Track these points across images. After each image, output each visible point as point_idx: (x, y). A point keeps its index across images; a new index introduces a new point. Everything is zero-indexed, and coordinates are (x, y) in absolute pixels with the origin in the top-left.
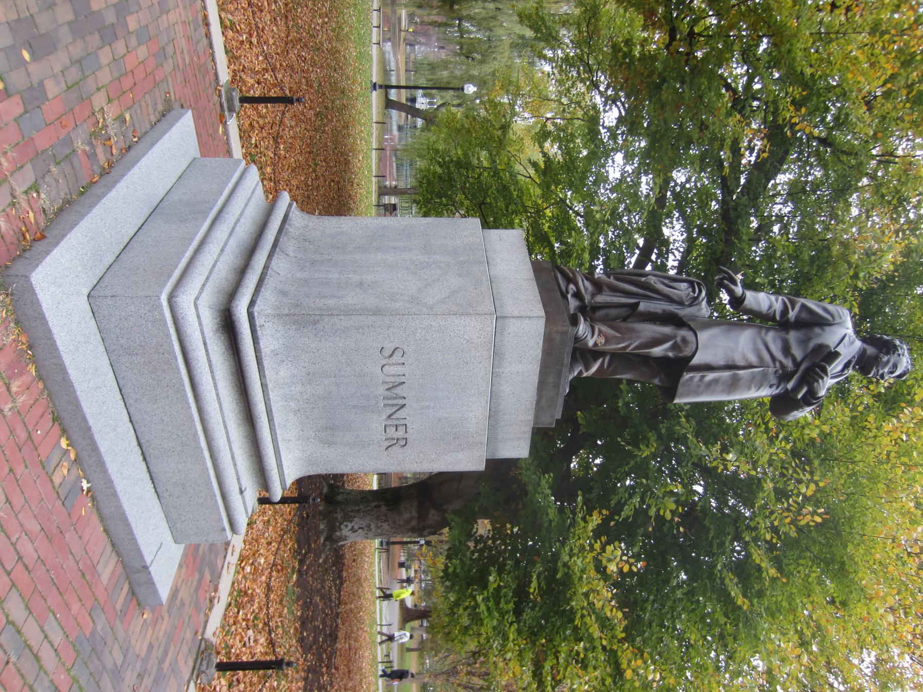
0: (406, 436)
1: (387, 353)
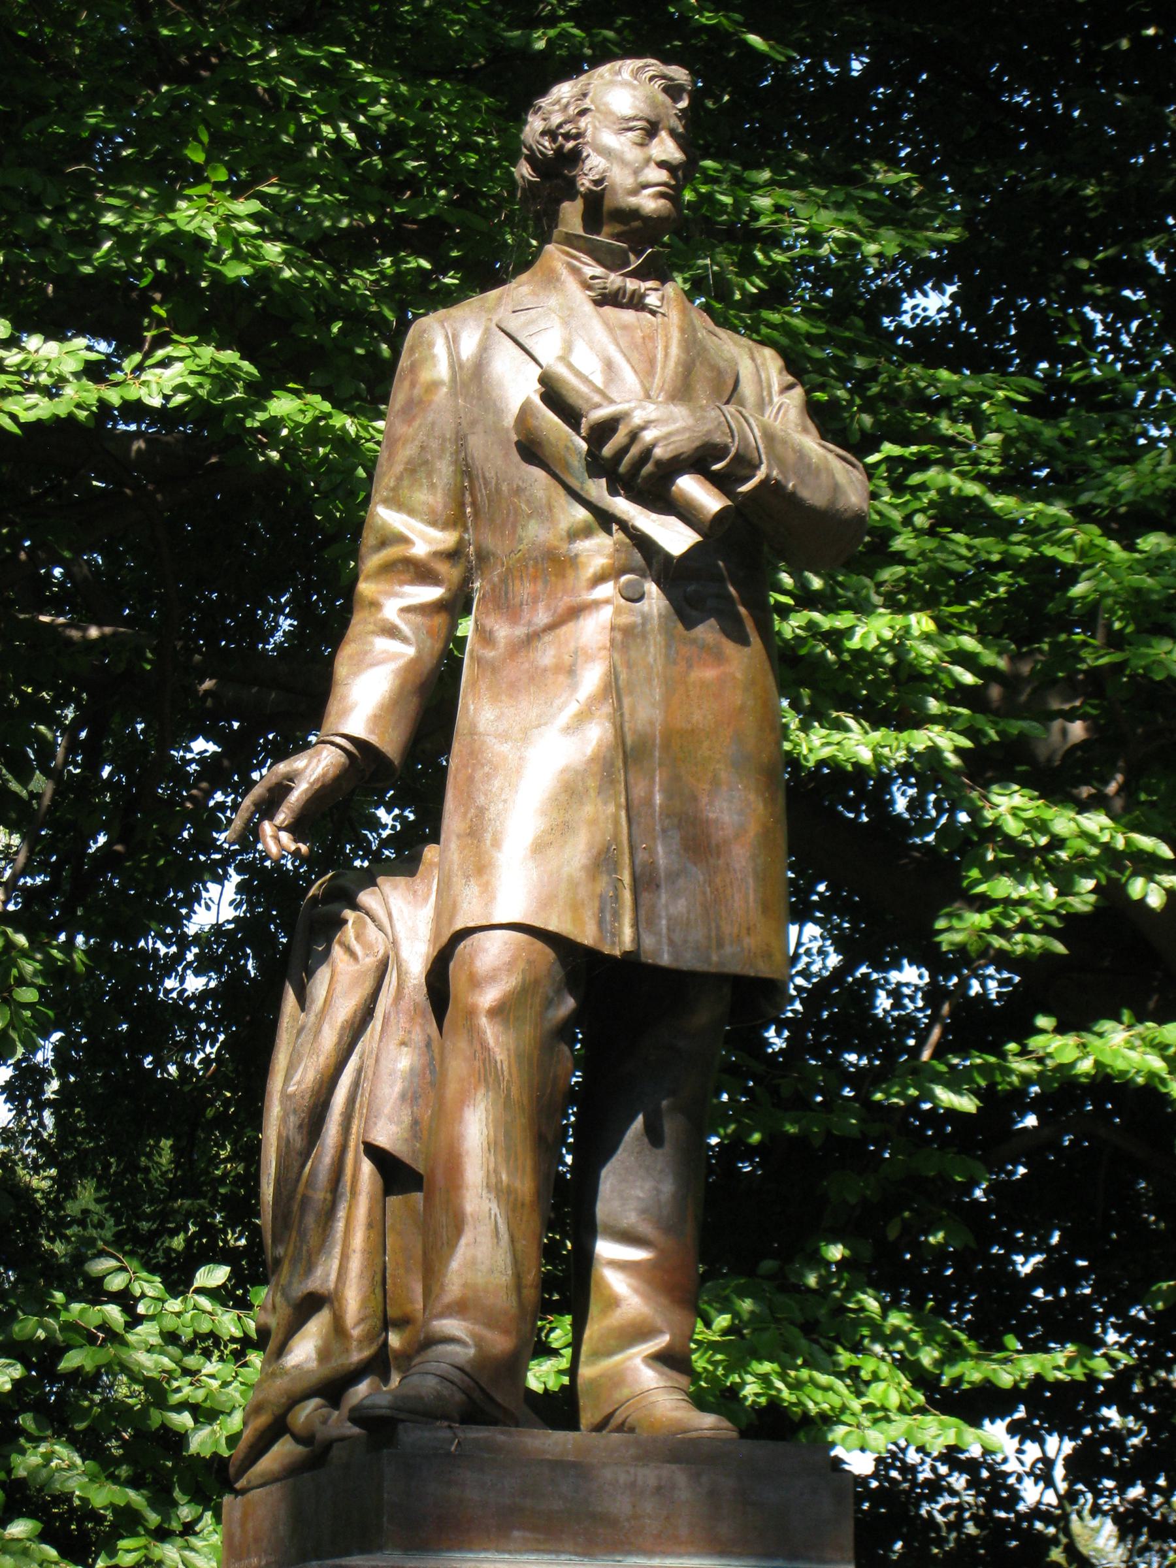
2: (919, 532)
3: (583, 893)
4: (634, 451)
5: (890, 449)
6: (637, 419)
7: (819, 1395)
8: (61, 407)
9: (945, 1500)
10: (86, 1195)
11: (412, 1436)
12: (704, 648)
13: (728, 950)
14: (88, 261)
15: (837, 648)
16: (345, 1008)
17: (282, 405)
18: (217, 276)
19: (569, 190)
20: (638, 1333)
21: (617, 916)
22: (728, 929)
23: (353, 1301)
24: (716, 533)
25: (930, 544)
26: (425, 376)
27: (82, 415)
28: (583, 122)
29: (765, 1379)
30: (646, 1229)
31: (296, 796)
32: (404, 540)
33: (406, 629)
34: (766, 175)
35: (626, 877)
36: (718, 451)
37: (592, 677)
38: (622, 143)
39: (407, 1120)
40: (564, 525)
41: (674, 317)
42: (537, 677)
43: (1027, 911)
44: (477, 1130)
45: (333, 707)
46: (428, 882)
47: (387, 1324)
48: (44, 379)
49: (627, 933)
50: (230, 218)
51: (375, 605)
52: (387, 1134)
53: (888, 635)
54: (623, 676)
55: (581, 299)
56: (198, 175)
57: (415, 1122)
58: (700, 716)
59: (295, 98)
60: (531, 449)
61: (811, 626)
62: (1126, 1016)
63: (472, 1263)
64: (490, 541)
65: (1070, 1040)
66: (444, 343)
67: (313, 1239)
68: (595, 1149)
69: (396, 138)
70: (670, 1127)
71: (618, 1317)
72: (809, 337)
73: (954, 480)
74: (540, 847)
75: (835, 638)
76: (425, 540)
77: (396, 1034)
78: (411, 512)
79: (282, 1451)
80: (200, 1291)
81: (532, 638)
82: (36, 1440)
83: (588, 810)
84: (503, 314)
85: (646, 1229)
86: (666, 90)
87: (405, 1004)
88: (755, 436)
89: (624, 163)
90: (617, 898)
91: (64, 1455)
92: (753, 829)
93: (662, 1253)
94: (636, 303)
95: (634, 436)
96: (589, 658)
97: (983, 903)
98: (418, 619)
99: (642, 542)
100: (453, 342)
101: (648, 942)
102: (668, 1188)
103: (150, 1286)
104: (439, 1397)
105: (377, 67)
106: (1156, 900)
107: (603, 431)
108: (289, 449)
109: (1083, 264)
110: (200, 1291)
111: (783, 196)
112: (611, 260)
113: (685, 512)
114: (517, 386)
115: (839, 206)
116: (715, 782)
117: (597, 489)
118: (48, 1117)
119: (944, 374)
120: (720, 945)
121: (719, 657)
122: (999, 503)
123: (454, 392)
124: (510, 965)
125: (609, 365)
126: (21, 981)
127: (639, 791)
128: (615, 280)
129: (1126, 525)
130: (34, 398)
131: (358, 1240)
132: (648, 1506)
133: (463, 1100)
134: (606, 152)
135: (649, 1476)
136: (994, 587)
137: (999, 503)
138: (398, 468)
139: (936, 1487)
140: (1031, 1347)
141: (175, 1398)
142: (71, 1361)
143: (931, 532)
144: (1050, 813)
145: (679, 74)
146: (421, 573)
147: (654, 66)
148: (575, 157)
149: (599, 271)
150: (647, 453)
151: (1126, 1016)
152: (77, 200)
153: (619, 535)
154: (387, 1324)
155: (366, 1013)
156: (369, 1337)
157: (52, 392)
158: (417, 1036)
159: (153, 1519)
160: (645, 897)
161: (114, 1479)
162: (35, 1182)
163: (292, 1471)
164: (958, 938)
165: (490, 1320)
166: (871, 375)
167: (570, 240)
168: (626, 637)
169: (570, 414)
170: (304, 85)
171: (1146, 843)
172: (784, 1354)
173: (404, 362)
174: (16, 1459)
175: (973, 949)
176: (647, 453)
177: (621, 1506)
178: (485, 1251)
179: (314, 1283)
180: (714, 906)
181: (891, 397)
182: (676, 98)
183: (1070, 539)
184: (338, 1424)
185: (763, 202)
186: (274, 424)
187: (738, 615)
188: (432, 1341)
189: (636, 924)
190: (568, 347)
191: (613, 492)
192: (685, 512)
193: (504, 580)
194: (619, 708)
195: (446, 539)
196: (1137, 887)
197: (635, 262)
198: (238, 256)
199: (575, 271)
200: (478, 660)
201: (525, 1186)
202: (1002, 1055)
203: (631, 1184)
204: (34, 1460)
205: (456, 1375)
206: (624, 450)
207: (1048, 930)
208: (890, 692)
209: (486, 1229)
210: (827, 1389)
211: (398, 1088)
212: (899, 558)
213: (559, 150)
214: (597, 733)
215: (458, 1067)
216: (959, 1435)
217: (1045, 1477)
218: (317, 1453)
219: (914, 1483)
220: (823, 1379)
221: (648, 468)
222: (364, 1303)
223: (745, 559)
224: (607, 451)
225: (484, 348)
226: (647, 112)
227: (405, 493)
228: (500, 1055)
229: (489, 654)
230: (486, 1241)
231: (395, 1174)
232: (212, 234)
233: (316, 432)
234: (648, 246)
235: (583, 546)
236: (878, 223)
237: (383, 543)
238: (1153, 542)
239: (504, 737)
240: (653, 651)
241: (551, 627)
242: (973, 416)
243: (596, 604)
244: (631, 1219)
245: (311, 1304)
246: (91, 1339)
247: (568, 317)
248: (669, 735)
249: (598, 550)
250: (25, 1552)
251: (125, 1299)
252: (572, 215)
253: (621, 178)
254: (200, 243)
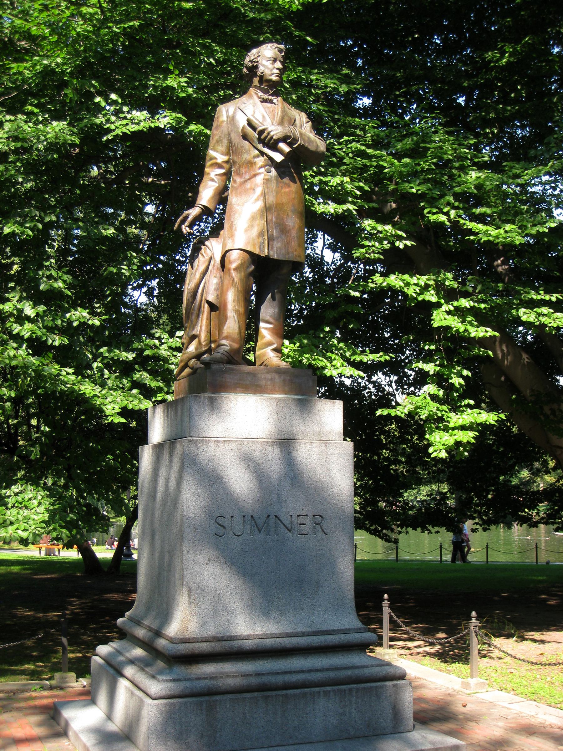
0: (310, 515)
1: (221, 531)
2: (350, 158)
3: (256, 241)
4: (269, 137)
5: (346, 138)
6: (269, 130)
7: (320, 362)
8: (139, 128)
9: (367, 390)
10: (165, 317)
11: (215, 367)
12: (286, 184)
13: (290, 255)
14: (147, 93)
15: (327, 186)
16: (202, 269)
17: (192, 127)
18: (178, 97)
19: (255, 75)
20: (269, 344)
21: (264, 247)
22: (290, 250)
23: (203, 337)
24: (287, 156)
25: (352, 161)
26: (221, 119)
27: (145, 129)
28: (259, 59)
29: (307, 358)
30: (271, 320)
31: (190, 219)
32: (216, 158)
33: (216, 180)
34: (316, 71)
35: (266, 238)
36: (289, 137)
37: (259, 190)
38: (268, 64)
39: (216, 295)
40: (253, 155)
41: (280, 105)
42: (246, 191)
43: (374, 248)
44: (231, 297)
45: (199, 198)
46: (220, 239)
47: (211, 342)
48: (136, 121)
49: (266, 251)
50: (180, 82)
51: (209, 174)
52: (211, 298)
53: (339, 182)
54: (266, 190)
55: (258, 101)
56: (172, 73)
57: (218, 295)
58: (284, 200)
59: (200, 53)
60: (245, 137)
61: (320, 180)
62: (397, 273)
63: (229, 327)
64: (236, 159)
65: (382, 278)
66: (225, 111)
67: (194, 322)
68: (260, 301)
69: (225, 62)
70: (277, 296)
71: (264, 341)
72: (324, 110)
73: (359, 146)
74: (246, 231)
75: (326, 183)
76: (221, 158)
77: (213, 275)
78: (217, 152)
79: (187, 371)
80: (177, 337)
81: (245, 182)
82: (139, 371)
83: (257, 222)
84: (239, 105)
85: (271, 320)
86: (279, 51)
87: (215, 268)
88: (298, 134)
89: (268, 68)
90: (264, 243)
91: (145, 374)
92: (297, 227)
93: (275, 325)
94: (271, 102)
95: (269, 134)
96: (258, 186)
97: (363, 246)
98: (219, 177)
99: (271, 159)
100: (227, 111)
101: (271, 253)
102: (276, 310)
103: (166, 336)
104: (221, 358)
105: (219, 44)
106: (402, 247)
107: (261, 132)
108: (194, 137)
109: (398, 93)
110: (177, 337)
111: (318, 77)
112: (265, 92)
113: (281, 152)
114: (242, 122)
115: (331, 79)
116: (288, 215)
117: (260, 146)
118: (155, 299)
119: (357, 119)
120: (288, 254)
121: (289, 186)
122: (369, 151)
123: (227, 124)
124: (238, 259)
125: (264, 117)
126: (134, 264)
127: (269, 218)
128: (266, 96)
129: (399, 156)
130: (134, 126)
131: (204, 322)
132: (269, 383)
133: (227, 290)
134: (264, 66)
135: (269, 376)
136: (370, 171)
137: (369, 151)
138: (214, 141)
139: (365, 387)
140: (371, 352)
141: (171, 362)
142: (147, 353)
143: (353, 158)
144: (377, 225)
145: (282, 47)
146: (220, 166)
147: (276, 45)
148: (256, 67)
149: (262, 94)
150: (272, 137)
151: (397, 273)
152: (145, 78)
153: (265, 157)
154: (211, 342)
155: (207, 270)
156: (206, 345)
157: (138, 124)
158: (218, 275)
159: (166, 389)
160: (271, 242)
161: (157, 380)
162: (153, 315)
163: (189, 375)
164: (358, 255)
165: (233, 340)
166: (339, 120)
167: (256, 87)
168: (267, 181)
169: (254, 129)
170: (202, 49)
171: (400, 233)
172: (311, 352)
173: (216, 116)
174: (134, 375)
175: (361, 257)
176: (272, 137)
177: (263, 383)
178: (232, 325)
179: (194, 332)
180: (287, 245)
181: (344, 125)
182: (281, 53)
183: (385, 159)
184: (199, 365)
185: (313, 78)
186: (191, 132)
187: (294, 177)
188: (219, 345)
189: (268, 249)
190: (254, 112)
191: (264, 147)
192: (281, 152)
193: (239, 168)
194: (265, 198)
195: (226, 158)
196: (397, 244)
197: (271, 92)
198: (182, 91)
199: (257, 94)
200: (233, 187)
201: (242, 310)
202: (368, 283)
203: (268, 310)
204: (138, 376)
205: (225, 353)
206: (267, 137)
207: (379, 253)
208: (339, 196)
209: (233, 319)
210: (322, 361)
211: (213, 287)
212: (345, 164)
213: (253, 65)
214: (260, 204)
215: (226, 282)
216: (354, 372)
217: (390, 385)
218: (195, 371)
219: (360, 387)
220: (321, 358)
221: (272, 141)
222: (206, 337)
223: (295, 163)
224: (262, 137)
225: (235, 113)
226: (274, 56)
227: (216, 147)
228: (236, 279)
229: (235, 185)
230: (233, 322)
231: (213, 307)
232: (176, 86)
233: (200, 133)
234: (273, 88)
235: (257, 160)
236: (341, 83)
237: (211, 159)
238: (406, 160)
239: (238, 205)
240: (273, 185)
241: (249, 179)
242: (363, 129)
243: (260, 173)
244: (268, 318)
245: (193, 337)
246: (152, 348)
247: (255, 105)
248: (277, 205)
249: (261, 161)
250: (135, 397)
251: (159, 339)
252: (256, 81)
253: (267, 72)
254: (173, 88)
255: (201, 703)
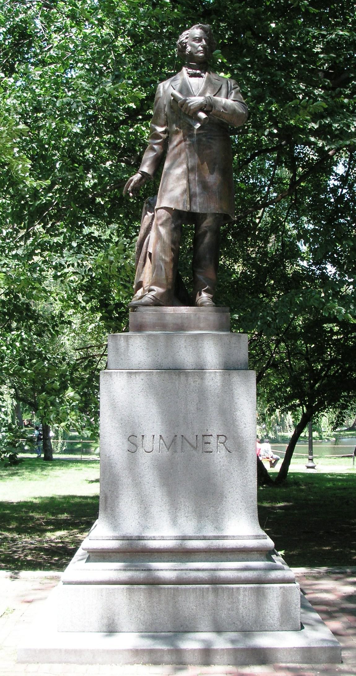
205: (152, 297)
255: (102, 589)
